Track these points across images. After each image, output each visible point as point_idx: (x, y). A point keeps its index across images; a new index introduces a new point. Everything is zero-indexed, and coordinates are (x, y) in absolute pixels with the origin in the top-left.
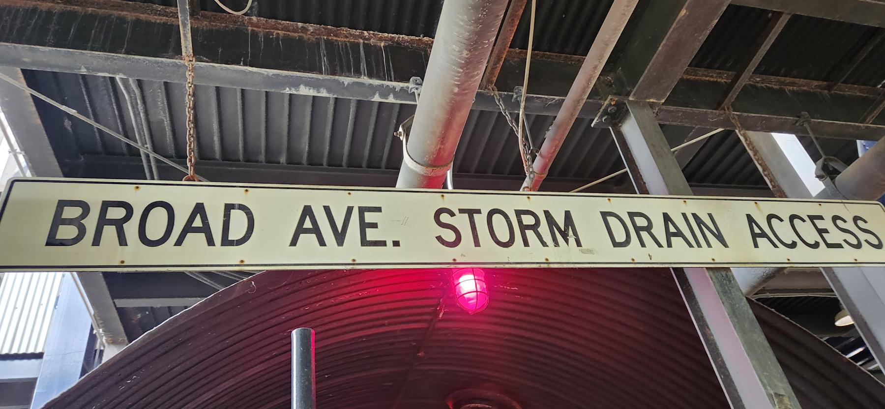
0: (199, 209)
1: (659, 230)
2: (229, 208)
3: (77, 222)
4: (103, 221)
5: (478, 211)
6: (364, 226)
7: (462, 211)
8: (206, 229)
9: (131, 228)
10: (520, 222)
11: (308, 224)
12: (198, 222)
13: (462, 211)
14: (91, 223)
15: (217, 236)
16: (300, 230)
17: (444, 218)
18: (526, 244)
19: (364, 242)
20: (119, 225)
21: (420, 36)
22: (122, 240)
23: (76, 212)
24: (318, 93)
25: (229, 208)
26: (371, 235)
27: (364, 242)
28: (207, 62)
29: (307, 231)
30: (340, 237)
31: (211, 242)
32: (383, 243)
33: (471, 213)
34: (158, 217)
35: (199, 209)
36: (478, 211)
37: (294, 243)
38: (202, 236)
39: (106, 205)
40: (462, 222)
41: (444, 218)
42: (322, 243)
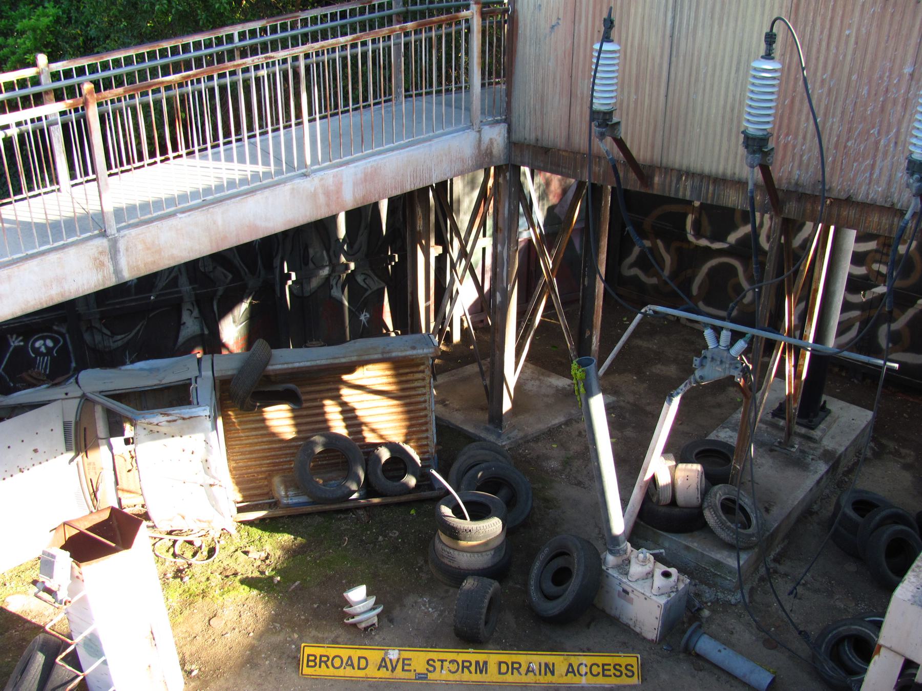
0: (350, 658)
1: (473, 668)
2: (359, 658)
3: (314, 661)
4: (321, 661)
5: (446, 661)
7: (438, 660)
8: (573, 672)
9: (329, 663)
10: (512, 666)
11: (349, 663)
12: (570, 670)
13: (438, 660)
14: (318, 660)
15: (356, 667)
16: (568, 672)
17: (431, 662)
18: (512, 674)
19: (403, 670)
20: (325, 662)
21: (35, 65)
22: (328, 667)
23: (325, 659)
24: (53, 556)
25: (359, 658)
26: (406, 668)
28: (798, 375)
29: (570, 672)
30: (394, 669)
31: (354, 668)
32: (410, 671)
33: (442, 661)
34: (363, 662)
35: (350, 658)
36: (446, 661)
37: (379, 669)
38: (385, 669)
39: (513, 663)
40: (438, 665)
41: (431, 662)
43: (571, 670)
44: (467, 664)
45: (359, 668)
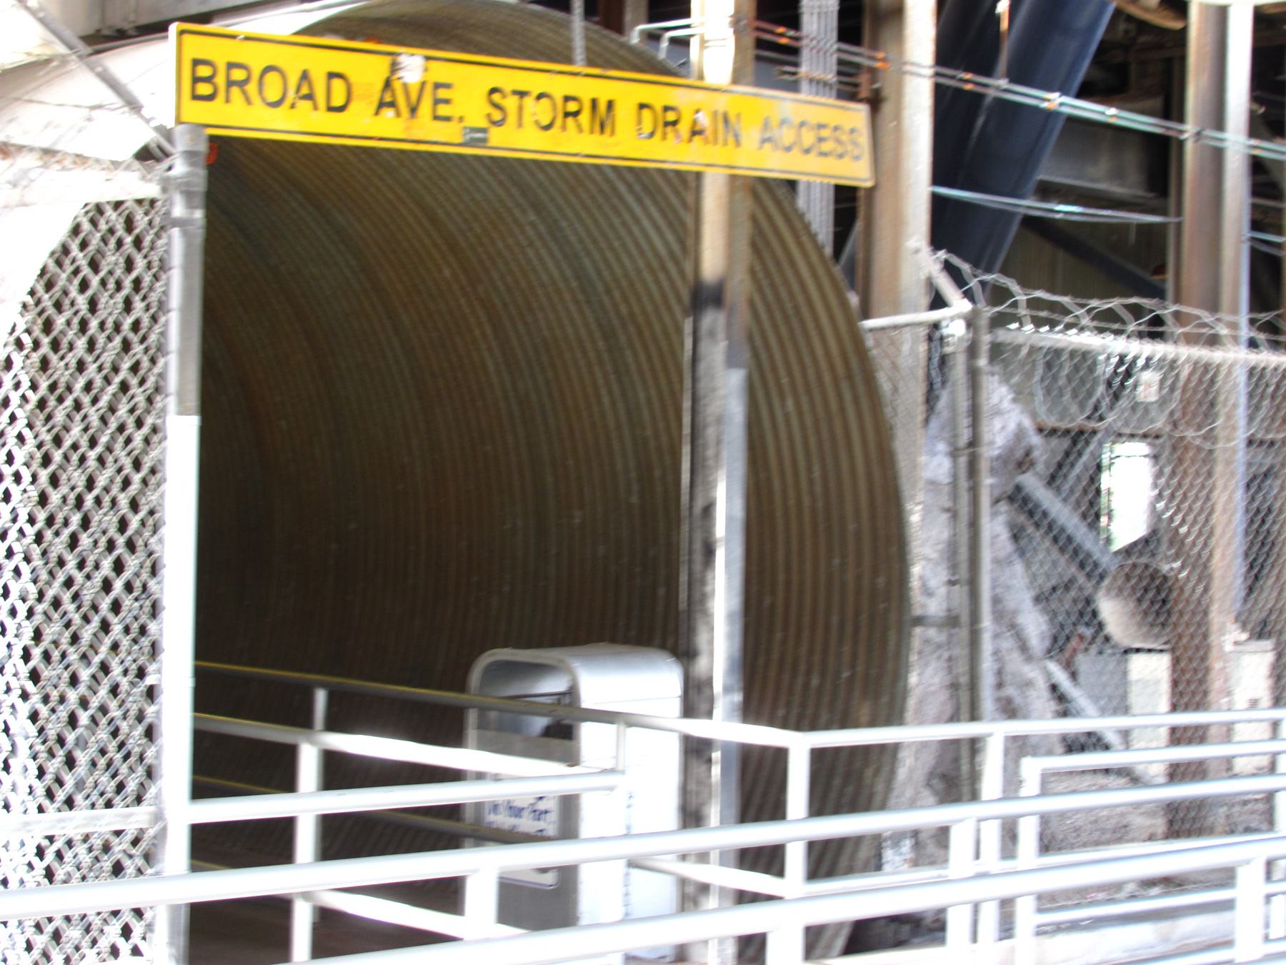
2: (332, 75)
6: (437, 102)
14: (220, 80)
27: (436, 118)
30: (413, 110)
42: (398, 114)
43: (603, 117)
44: (238, 75)
45: (331, 109)
